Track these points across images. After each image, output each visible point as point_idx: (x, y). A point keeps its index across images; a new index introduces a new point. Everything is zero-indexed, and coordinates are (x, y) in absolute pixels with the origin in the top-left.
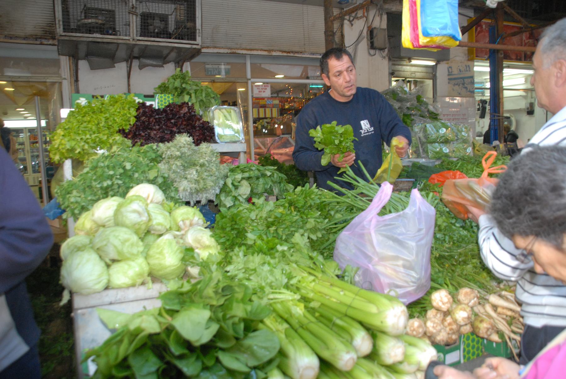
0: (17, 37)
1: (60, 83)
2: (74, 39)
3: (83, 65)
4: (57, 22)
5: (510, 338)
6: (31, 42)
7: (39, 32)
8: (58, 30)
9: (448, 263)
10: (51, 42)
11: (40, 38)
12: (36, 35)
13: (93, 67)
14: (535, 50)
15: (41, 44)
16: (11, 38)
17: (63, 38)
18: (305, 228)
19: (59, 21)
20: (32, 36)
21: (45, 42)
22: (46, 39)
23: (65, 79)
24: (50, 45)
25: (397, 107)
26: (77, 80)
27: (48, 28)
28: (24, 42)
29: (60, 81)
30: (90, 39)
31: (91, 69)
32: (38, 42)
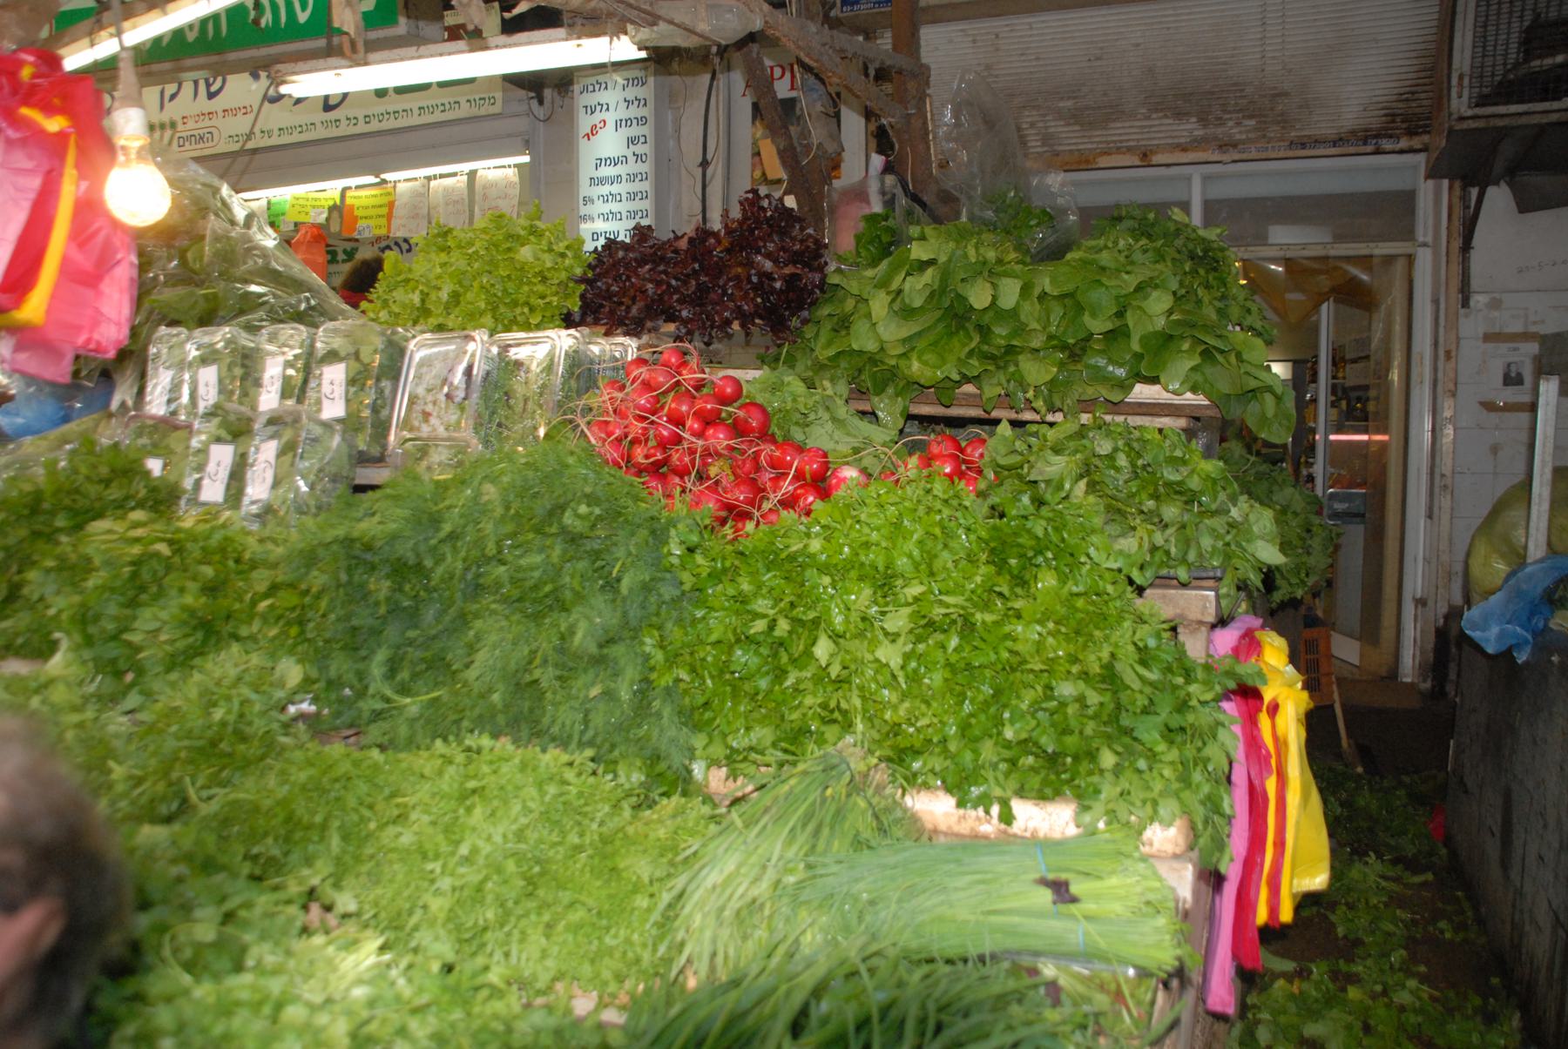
0: (1317, 142)
1: (1410, 259)
2: (1500, 123)
3: (1498, 198)
4: (1454, 81)
5: (1100, 935)
6: (1352, 150)
7: (1375, 120)
8: (1455, 102)
9: (652, 637)
10: (1404, 143)
11: (1377, 136)
12: (1366, 130)
13: (1526, 204)
14: (493, 41)
15: (1378, 152)
16: (1303, 146)
17: (1465, 125)
18: (1010, 604)
19: (1461, 77)
20: (1353, 132)
21: (1387, 145)
22: (1391, 136)
23: (1425, 245)
24: (1401, 152)
25: (1214, 238)
26: (1466, 247)
27: (1401, 105)
28: (1333, 151)
29: (1409, 251)
30: (1554, 117)
31: (1521, 212)
32: (1369, 148)
